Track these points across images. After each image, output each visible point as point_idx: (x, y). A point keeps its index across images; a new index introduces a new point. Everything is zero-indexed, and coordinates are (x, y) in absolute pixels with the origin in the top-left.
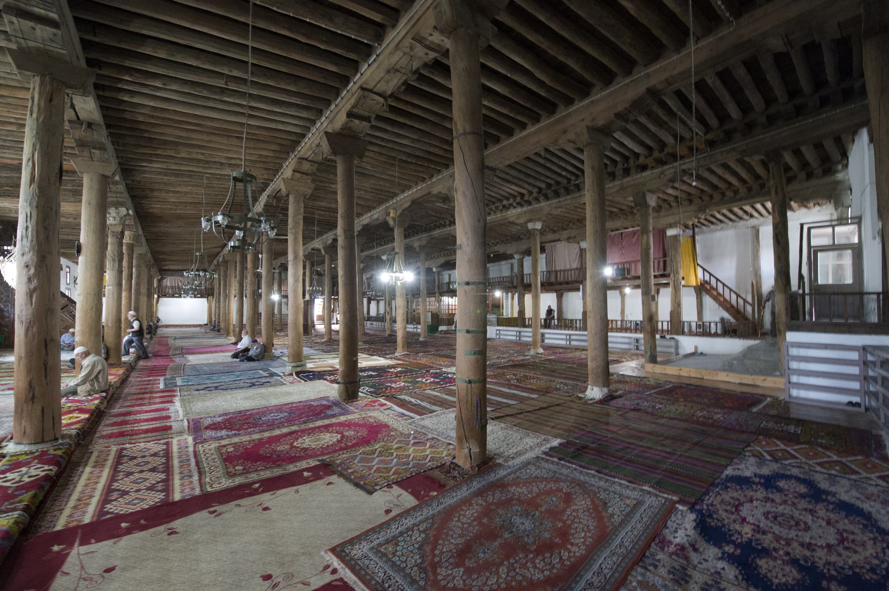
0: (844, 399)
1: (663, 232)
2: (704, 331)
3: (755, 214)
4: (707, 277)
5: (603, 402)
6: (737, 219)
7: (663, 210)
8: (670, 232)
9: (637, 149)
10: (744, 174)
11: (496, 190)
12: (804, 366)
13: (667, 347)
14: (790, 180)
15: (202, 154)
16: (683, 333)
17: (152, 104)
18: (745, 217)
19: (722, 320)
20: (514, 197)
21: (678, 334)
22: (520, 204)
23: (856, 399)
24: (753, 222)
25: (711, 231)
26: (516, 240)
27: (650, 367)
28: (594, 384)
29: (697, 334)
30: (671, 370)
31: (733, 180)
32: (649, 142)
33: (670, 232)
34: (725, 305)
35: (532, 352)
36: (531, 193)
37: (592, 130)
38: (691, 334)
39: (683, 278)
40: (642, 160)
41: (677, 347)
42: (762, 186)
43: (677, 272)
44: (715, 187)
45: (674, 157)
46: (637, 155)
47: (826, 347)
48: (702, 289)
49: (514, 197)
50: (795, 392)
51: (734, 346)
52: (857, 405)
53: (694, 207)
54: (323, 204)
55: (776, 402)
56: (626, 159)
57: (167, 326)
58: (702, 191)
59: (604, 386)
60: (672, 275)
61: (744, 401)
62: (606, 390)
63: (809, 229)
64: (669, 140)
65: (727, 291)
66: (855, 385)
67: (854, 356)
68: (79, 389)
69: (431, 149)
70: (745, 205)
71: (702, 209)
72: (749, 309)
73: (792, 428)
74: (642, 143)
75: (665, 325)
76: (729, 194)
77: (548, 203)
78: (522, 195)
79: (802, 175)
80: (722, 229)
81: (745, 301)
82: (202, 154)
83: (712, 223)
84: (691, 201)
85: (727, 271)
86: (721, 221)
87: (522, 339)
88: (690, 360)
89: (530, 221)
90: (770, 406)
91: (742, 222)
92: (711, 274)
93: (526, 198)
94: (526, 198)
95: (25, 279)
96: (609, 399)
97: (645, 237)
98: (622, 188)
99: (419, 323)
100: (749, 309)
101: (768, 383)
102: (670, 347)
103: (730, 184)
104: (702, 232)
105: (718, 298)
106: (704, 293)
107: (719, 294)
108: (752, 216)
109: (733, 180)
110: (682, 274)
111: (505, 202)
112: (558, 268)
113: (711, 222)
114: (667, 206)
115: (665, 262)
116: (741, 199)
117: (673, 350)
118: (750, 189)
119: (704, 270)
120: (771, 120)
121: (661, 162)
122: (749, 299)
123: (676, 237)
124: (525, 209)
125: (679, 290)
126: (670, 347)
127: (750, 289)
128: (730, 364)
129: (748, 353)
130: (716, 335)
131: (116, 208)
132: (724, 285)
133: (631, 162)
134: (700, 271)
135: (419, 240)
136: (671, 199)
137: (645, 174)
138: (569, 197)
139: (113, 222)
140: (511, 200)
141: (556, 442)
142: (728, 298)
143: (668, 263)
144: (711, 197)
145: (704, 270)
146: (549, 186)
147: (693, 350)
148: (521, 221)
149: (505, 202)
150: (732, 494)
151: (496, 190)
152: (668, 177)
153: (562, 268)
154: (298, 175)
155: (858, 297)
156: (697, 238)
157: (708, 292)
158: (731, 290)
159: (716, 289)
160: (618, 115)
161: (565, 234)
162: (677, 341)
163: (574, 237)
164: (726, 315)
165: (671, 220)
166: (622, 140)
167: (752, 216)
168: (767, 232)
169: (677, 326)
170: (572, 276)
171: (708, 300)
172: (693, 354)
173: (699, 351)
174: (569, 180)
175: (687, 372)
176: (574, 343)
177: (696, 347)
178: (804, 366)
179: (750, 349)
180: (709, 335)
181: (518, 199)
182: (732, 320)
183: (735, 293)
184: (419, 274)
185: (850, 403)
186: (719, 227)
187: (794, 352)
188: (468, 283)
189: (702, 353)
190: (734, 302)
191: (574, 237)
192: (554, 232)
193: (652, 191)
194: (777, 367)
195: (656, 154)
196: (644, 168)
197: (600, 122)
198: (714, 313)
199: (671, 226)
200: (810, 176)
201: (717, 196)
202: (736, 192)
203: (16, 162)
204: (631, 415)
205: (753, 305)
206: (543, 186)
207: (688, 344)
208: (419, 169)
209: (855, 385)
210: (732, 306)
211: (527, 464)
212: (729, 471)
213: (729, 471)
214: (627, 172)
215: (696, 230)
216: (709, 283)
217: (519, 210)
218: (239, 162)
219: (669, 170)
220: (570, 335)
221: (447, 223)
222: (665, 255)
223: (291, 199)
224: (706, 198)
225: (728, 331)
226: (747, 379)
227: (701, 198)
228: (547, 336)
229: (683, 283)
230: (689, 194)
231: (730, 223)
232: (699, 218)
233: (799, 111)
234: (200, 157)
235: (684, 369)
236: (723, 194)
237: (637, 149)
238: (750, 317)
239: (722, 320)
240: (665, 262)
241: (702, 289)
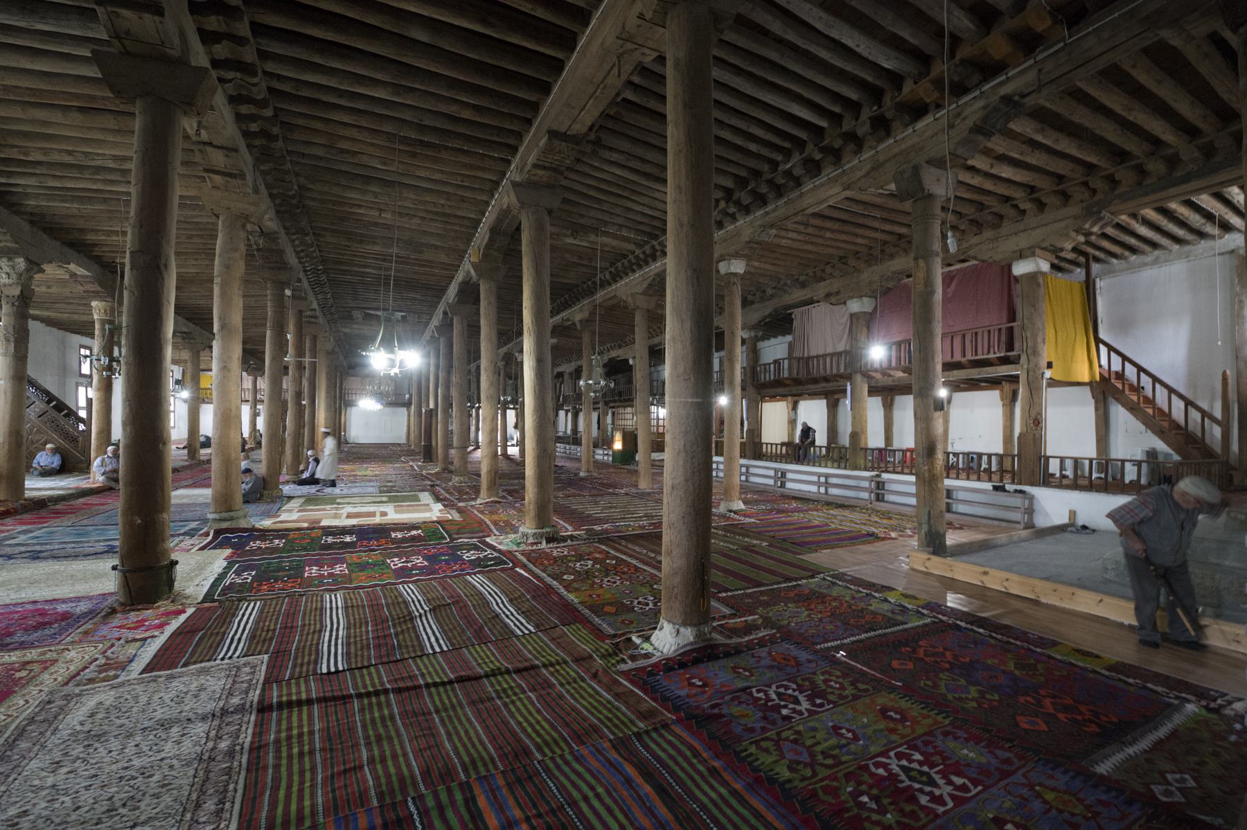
4: (1116, 364)
6: (1189, 237)
7: (1005, 223)
8: (1020, 269)
9: (888, 61)
10: (1185, 107)
11: (646, 200)
13: (1008, 508)
15: (69, 153)
17: (28, 84)
18: (1209, 228)
25: (1132, 268)
31: (1157, 127)
33: (1020, 269)
34: (1158, 422)
39: (1050, 365)
41: (1030, 511)
43: (1035, 352)
44: (1120, 155)
45: (990, 69)
46: (896, 79)
53: (1073, 210)
54: (377, 248)
56: (876, 94)
57: (1008, 439)
58: (1090, 167)
59: (685, 624)
60: (1023, 359)
62: (688, 634)
69: (452, 109)
70: (1199, 191)
74: (895, 43)
76: (1156, 167)
77: (749, 218)
80: (1156, 262)
81: (1204, 414)
82: (69, 153)
83: (1133, 250)
84: (1065, 197)
86: (1155, 245)
87: (752, 479)
91: (1204, 244)
92: (1125, 358)
98: (877, 167)
99: (580, 444)
103: (1156, 142)
104: (1112, 272)
105: (1144, 410)
106: (1111, 400)
109: (1157, 127)
112: (813, 353)
113: (1129, 246)
114: (1013, 212)
116: (1186, 179)
118: (1209, 152)
119: (1111, 349)
123: (1033, 277)
125: (1039, 389)
131: (10, 259)
135: (581, 310)
136: (1018, 194)
138: (781, 202)
139: (7, 281)
144: (1113, 182)
145: (1111, 349)
146: (742, 182)
147: (1064, 520)
151: (646, 200)
152: (969, 123)
153: (821, 352)
157: (1120, 397)
161: (821, 289)
162: (1031, 498)
163: (838, 293)
164: (1160, 446)
165: (1023, 241)
166: (835, 34)
170: (830, 368)
171: (1120, 415)
172: (1062, 529)
173: (1080, 522)
174: (774, 165)
176: (833, 491)
177: (1073, 514)
183: (1181, 396)
184: (427, 355)
186: (1149, 259)
189: (1084, 527)
191: (838, 293)
192: (803, 285)
193: (939, 163)
196: (918, 111)
199: (1021, 255)
201: (1125, 175)
202: (1173, 162)
206: (729, 183)
208: (466, 160)
210: (1176, 425)
214: (882, 126)
215: (1095, 267)
216: (1120, 376)
218: (127, 166)
219: (973, 106)
220: (827, 476)
222: (1012, 317)
224: (1097, 183)
227: (1086, 184)
228: (789, 476)
229: (1048, 374)
230: (1060, 178)
231: (1176, 247)
232: (1088, 234)
234: (68, 159)
235: (993, 572)
237: (888, 61)
238: (1218, 448)
239: (1152, 454)
241: (1106, 390)
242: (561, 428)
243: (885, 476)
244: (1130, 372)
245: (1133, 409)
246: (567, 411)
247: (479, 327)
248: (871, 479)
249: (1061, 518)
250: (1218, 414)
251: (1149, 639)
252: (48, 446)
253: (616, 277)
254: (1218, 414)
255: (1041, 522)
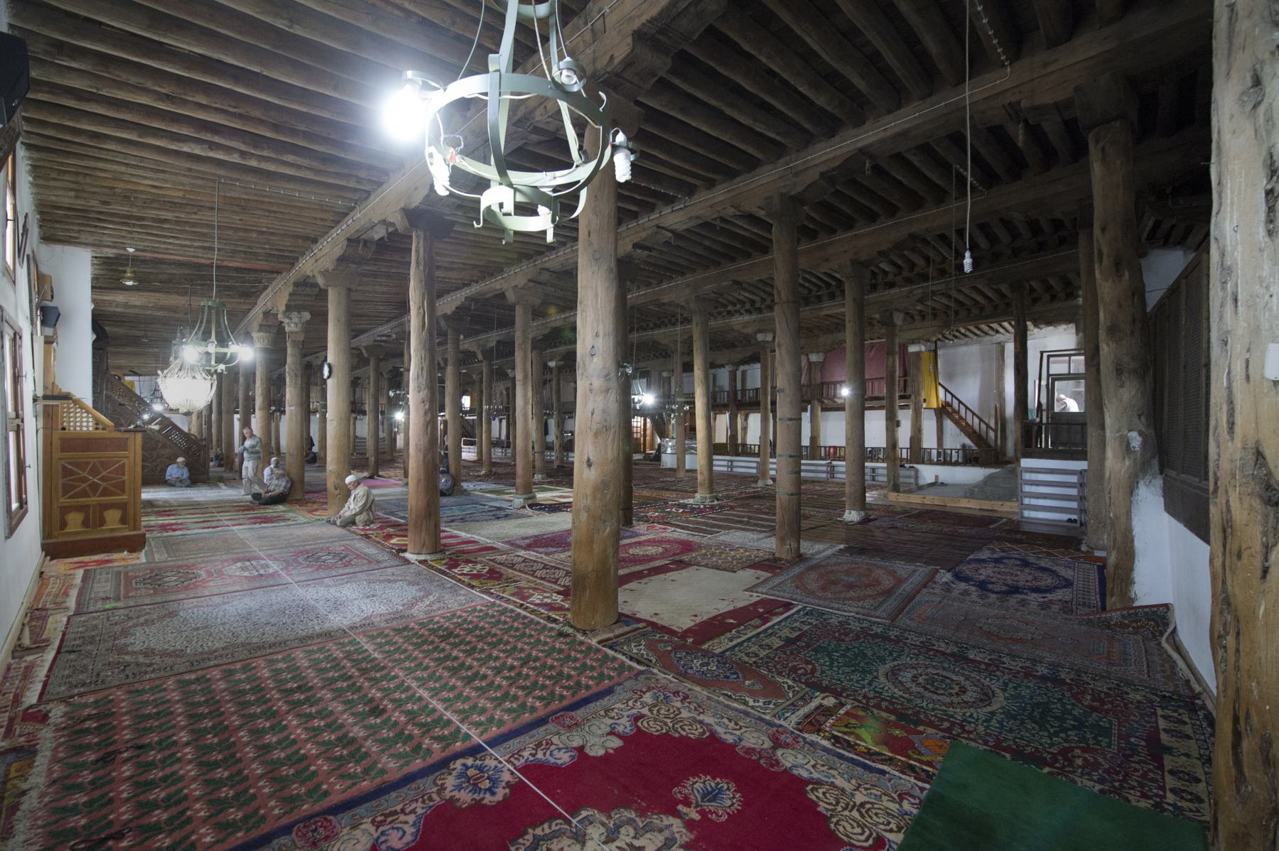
0: (1065, 517)
1: (904, 348)
2: (944, 460)
3: (1001, 330)
4: (949, 398)
5: (861, 523)
8: (913, 349)
12: (1034, 489)
14: (1035, 301)
16: (923, 463)
19: (964, 446)
20: (743, 303)
21: (918, 463)
22: (749, 312)
23: (1074, 517)
24: (999, 338)
25: (954, 346)
26: (728, 348)
27: (893, 497)
28: (851, 509)
29: (938, 463)
30: (915, 499)
31: (979, 298)
32: (900, 262)
33: (913, 349)
35: (760, 484)
36: (763, 300)
37: (854, 262)
38: (931, 463)
40: (890, 278)
41: (917, 477)
42: (1008, 305)
43: (919, 394)
45: (925, 277)
46: (886, 273)
47: (1052, 471)
48: (944, 412)
49: (743, 303)
50: (1026, 513)
51: (972, 475)
52: (1075, 521)
55: (1011, 521)
61: (983, 521)
63: (1049, 357)
64: (920, 262)
65: (969, 415)
66: (1074, 505)
67: (1074, 479)
68: (358, 518)
71: (947, 325)
72: (992, 434)
73: (1019, 536)
75: (904, 451)
76: (975, 311)
78: (753, 302)
79: (1047, 297)
80: (966, 344)
81: (988, 426)
85: (969, 392)
86: (966, 336)
87: (735, 470)
88: (932, 490)
89: (760, 331)
90: (1006, 524)
91: (987, 338)
92: (953, 396)
93: (758, 305)
94: (758, 305)
95: (422, 413)
96: (865, 521)
97: (891, 359)
100: (992, 434)
101: (1006, 508)
102: (909, 477)
104: (945, 347)
107: (961, 418)
108: (997, 332)
109: (979, 298)
110: (923, 396)
111: (730, 308)
115: (905, 381)
117: (912, 481)
118: (996, 307)
119: (946, 390)
120: (1016, 252)
121: (909, 281)
122: (992, 425)
123: (918, 354)
124: (753, 317)
126: (909, 477)
127: (993, 412)
128: (971, 491)
129: (988, 480)
130: (957, 464)
132: (967, 408)
133: (880, 277)
134: (941, 391)
137: (892, 291)
140: (738, 306)
141: (842, 546)
142: (970, 422)
143: (909, 383)
144: (957, 313)
145: (946, 390)
148: (749, 330)
149: (730, 308)
150: (973, 565)
154: (531, 284)
155: (1079, 428)
156: (939, 352)
157: (950, 416)
158: (974, 414)
159: (958, 412)
160: (881, 253)
162: (917, 471)
164: (968, 442)
165: (914, 334)
167: (997, 332)
168: (1010, 348)
169: (918, 454)
171: (948, 424)
173: (940, 480)
175: (930, 500)
177: (937, 477)
178: (1034, 489)
179: (990, 477)
180: (950, 463)
181: (748, 306)
182: (974, 447)
185: (1070, 520)
187: (1027, 476)
188: (790, 419)
190: (976, 427)
194: (1013, 493)
195: (906, 273)
196: (891, 285)
197: (863, 257)
198: (955, 439)
199: (913, 342)
200: (1053, 298)
203: (208, 262)
204: (890, 531)
205: (995, 431)
207: (928, 473)
209: (1074, 505)
211: (829, 557)
212: (971, 557)
213: (971, 557)
216: (950, 405)
217: (747, 318)
219: (918, 289)
221: (651, 325)
223: (519, 311)
225: (970, 459)
226: (987, 505)
233: (1041, 247)
236: (969, 310)
238: (992, 444)
239: (964, 446)
240: (905, 381)
241: (944, 412)
242: (495, 434)
243: (834, 463)
244: (955, 404)
245: (957, 423)
246: (500, 421)
247: (326, 314)
248: (827, 465)
249: (931, 480)
250: (993, 426)
251: (1226, 52)
252: (180, 459)
253: (657, 326)
254: (993, 426)
255: (921, 482)
